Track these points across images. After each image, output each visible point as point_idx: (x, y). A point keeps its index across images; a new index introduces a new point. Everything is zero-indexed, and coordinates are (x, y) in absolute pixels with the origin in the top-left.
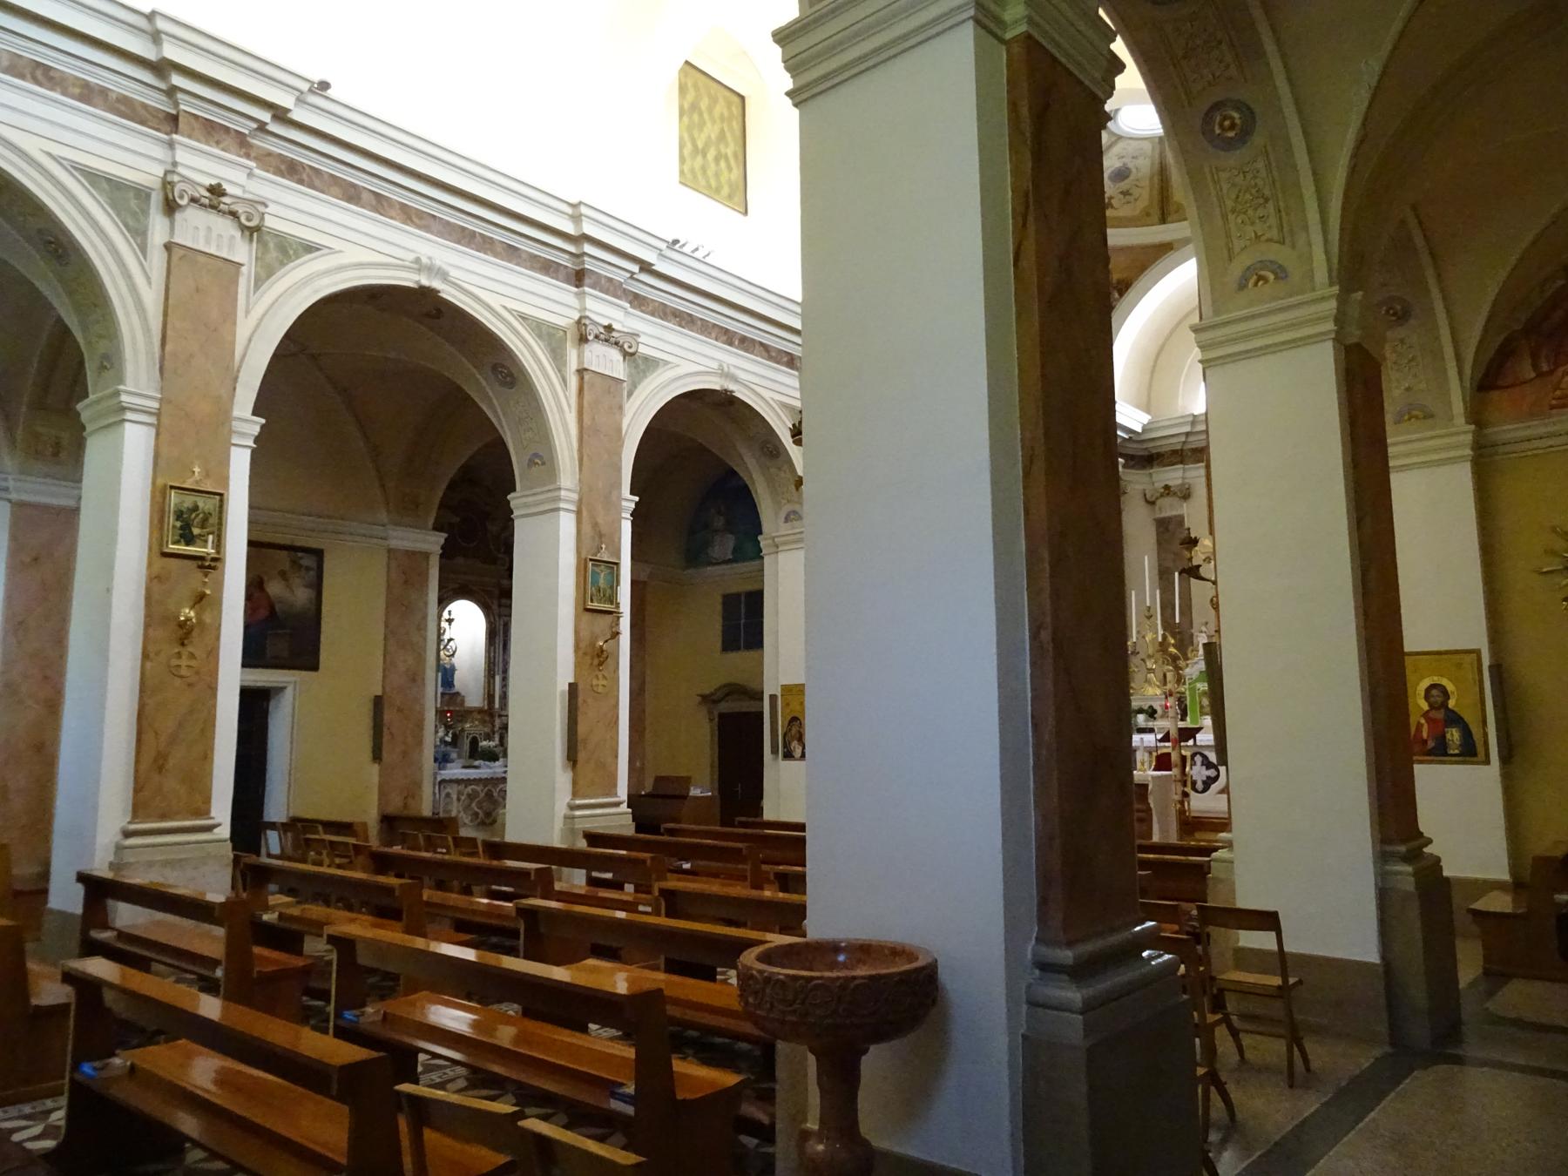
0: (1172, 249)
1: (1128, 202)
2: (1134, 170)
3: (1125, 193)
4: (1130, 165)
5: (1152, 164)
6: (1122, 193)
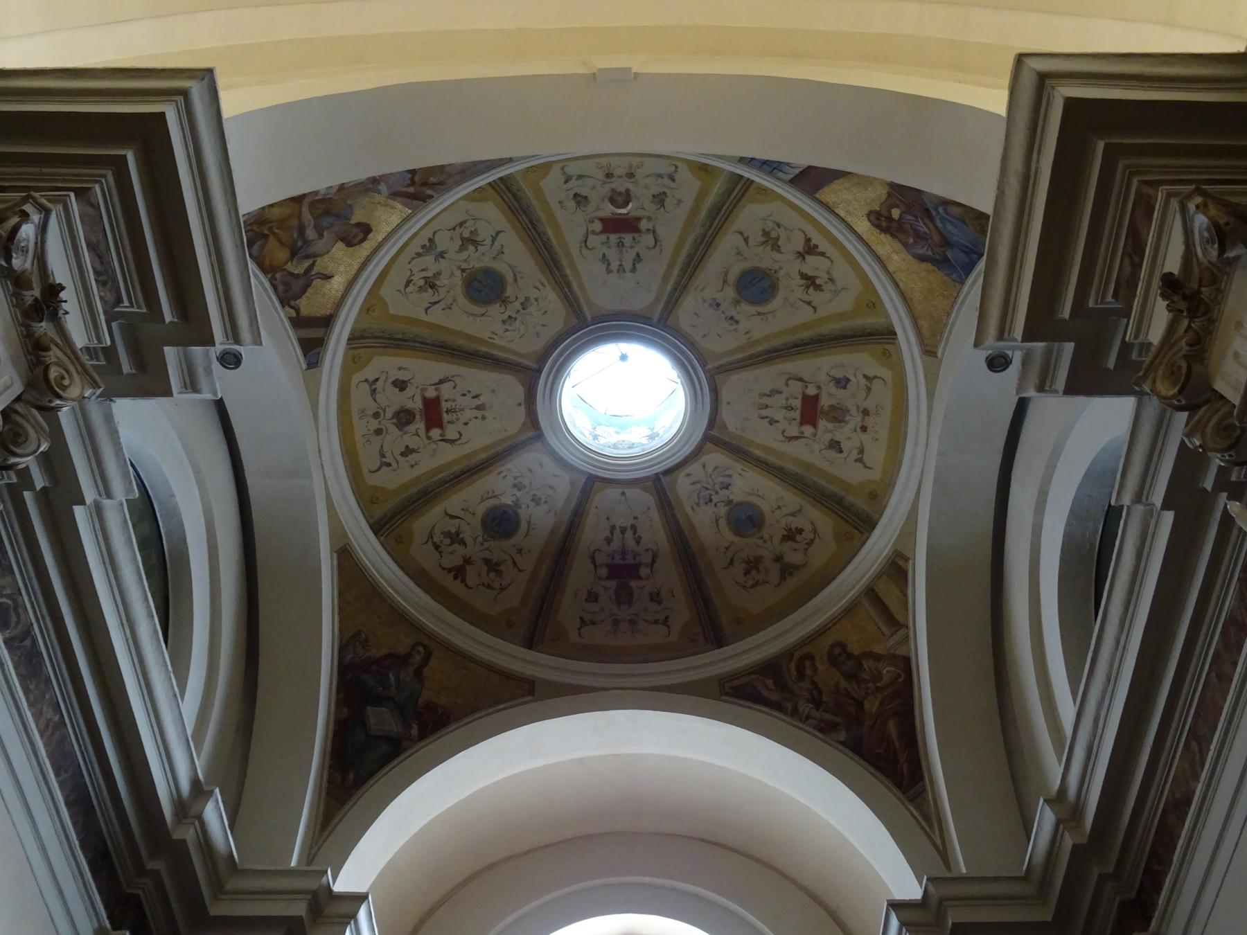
0: (531, 692)
1: (489, 587)
2: (523, 527)
3: (493, 567)
4: (523, 513)
5: (553, 532)
6: (487, 561)
